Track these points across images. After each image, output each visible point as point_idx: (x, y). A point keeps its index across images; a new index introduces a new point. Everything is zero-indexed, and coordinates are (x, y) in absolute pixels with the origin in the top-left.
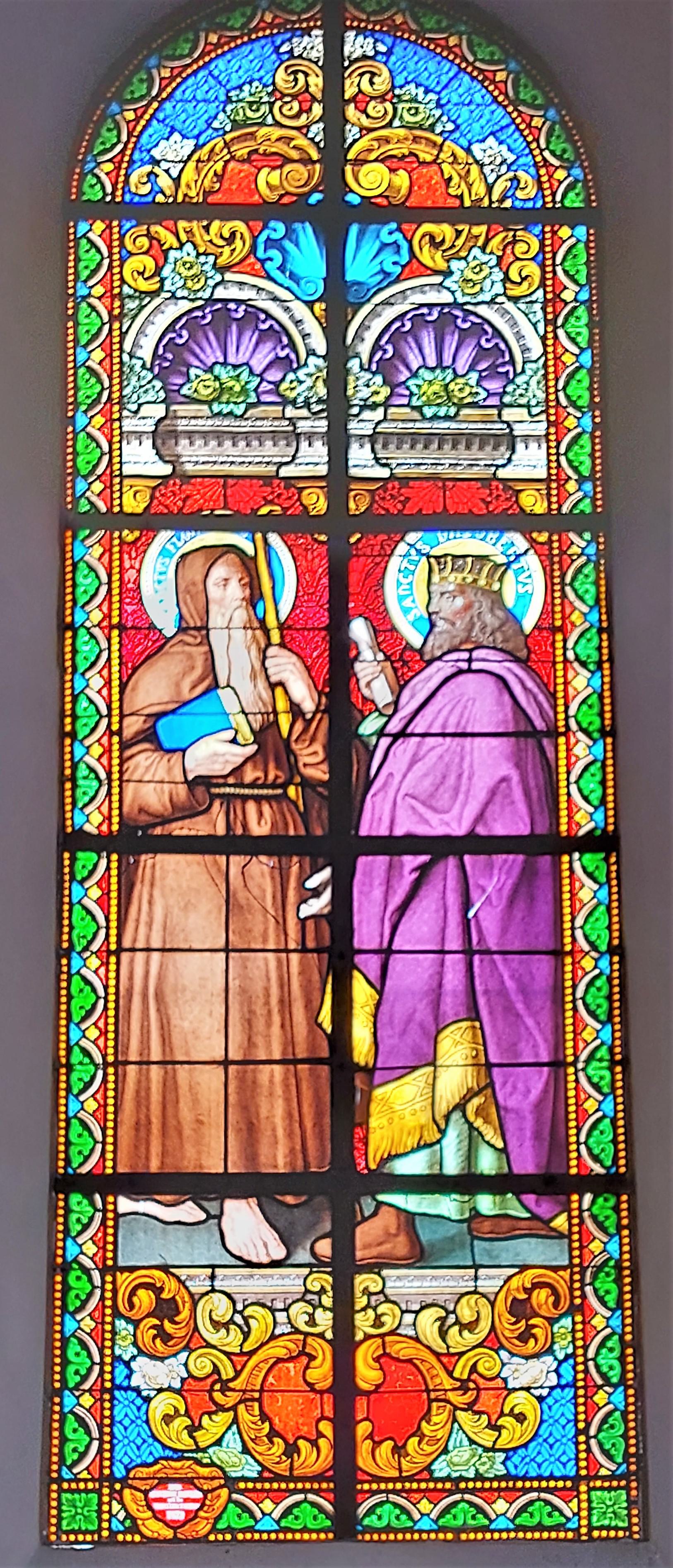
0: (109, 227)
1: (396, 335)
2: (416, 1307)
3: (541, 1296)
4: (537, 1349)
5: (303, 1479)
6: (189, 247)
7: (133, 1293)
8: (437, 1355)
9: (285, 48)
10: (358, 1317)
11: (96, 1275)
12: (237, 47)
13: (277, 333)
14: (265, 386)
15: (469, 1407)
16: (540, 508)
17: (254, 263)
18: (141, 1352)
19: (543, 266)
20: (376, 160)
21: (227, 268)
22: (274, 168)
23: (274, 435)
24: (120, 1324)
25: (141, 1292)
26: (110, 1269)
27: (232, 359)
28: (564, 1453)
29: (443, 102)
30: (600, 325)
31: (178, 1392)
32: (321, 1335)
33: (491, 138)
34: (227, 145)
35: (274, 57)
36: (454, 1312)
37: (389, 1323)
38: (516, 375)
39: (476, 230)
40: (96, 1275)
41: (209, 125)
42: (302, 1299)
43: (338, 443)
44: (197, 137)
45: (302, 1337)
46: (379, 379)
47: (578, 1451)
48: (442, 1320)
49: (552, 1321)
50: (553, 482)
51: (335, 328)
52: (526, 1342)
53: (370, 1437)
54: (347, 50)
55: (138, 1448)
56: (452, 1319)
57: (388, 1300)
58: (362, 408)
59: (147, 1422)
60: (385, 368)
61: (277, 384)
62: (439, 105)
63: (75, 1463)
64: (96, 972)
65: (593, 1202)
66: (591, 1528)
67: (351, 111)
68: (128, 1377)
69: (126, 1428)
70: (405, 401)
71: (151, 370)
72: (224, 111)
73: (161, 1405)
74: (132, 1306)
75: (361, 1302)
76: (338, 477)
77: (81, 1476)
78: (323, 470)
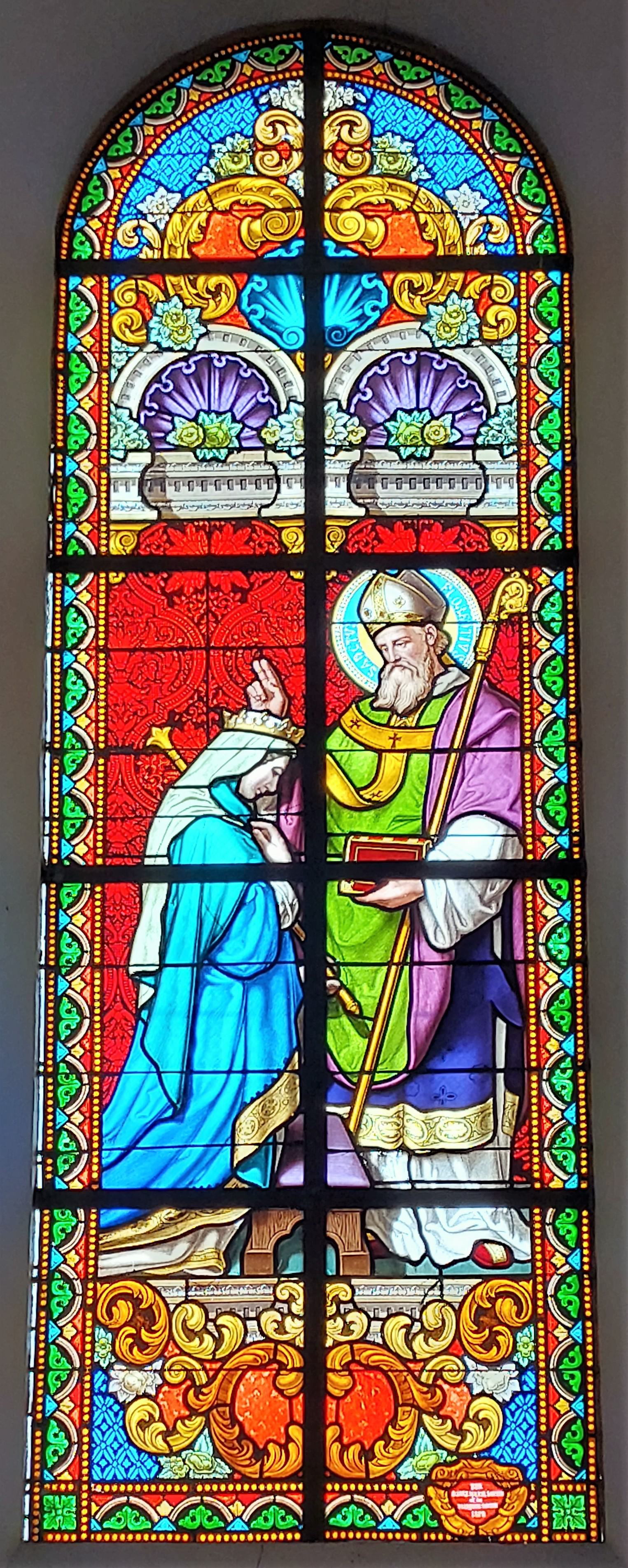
0: (101, 282)
1: (373, 379)
2: (383, 1315)
3: (506, 1307)
4: (501, 1354)
5: (273, 1480)
6: (176, 300)
7: (113, 1302)
8: (404, 1361)
9: (263, 100)
10: (329, 1324)
11: (78, 1284)
12: (219, 102)
13: (257, 380)
14: (247, 433)
15: (436, 1412)
16: (512, 544)
17: (236, 315)
18: (119, 1360)
19: (517, 310)
20: (352, 209)
21: (213, 321)
22: (255, 218)
23: (257, 481)
24: (100, 1332)
25: (121, 1303)
26: (90, 1278)
27: (214, 407)
28: (526, 1456)
29: (420, 151)
30: (571, 366)
31: (154, 1399)
32: (290, 1343)
33: (465, 185)
34: (210, 199)
35: (254, 109)
36: (420, 1320)
37: (358, 1331)
38: (489, 416)
39: (454, 276)
40: (78, 1284)
41: (194, 179)
42: (272, 1307)
43: (314, 482)
44: (182, 192)
45: (272, 1345)
46: (356, 420)
47: (539, 1454)
48: (409, 1327)
49: (514, 1331)
50: (524, 519)
51: (314, 373)
52: (488, 1350)
53: (339, 1439)
54: (326, 104)
55: (115, 1452)
56: (417, 1327)
57: (357, 1309)
58: (339, 448)
59: (124, 1427)
60: (359, 411)
61: (259, 430)
62: (415, 153)
63: (56, 1465)
64: (87, 604)
65: (556, 1217)
66: (552, 1532)
67: (329, 161)
68: (106, 1383)
69: (103, 1434)
70: (382, 442)
71: (137, 420)
72: (207, 165)
73: (137, 1412)
74: (110, 1315)
75: (331, 1310)
76: (314, 518)
77: (62, 1478)
78: (301, 510)
